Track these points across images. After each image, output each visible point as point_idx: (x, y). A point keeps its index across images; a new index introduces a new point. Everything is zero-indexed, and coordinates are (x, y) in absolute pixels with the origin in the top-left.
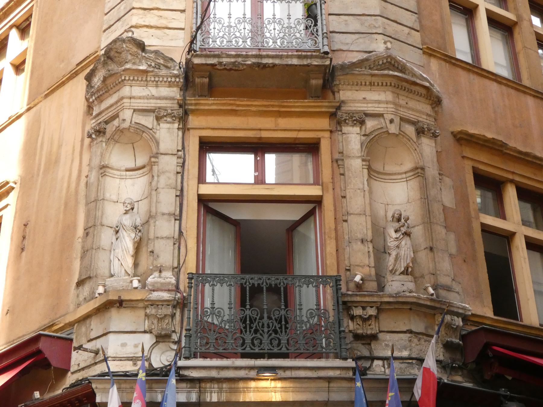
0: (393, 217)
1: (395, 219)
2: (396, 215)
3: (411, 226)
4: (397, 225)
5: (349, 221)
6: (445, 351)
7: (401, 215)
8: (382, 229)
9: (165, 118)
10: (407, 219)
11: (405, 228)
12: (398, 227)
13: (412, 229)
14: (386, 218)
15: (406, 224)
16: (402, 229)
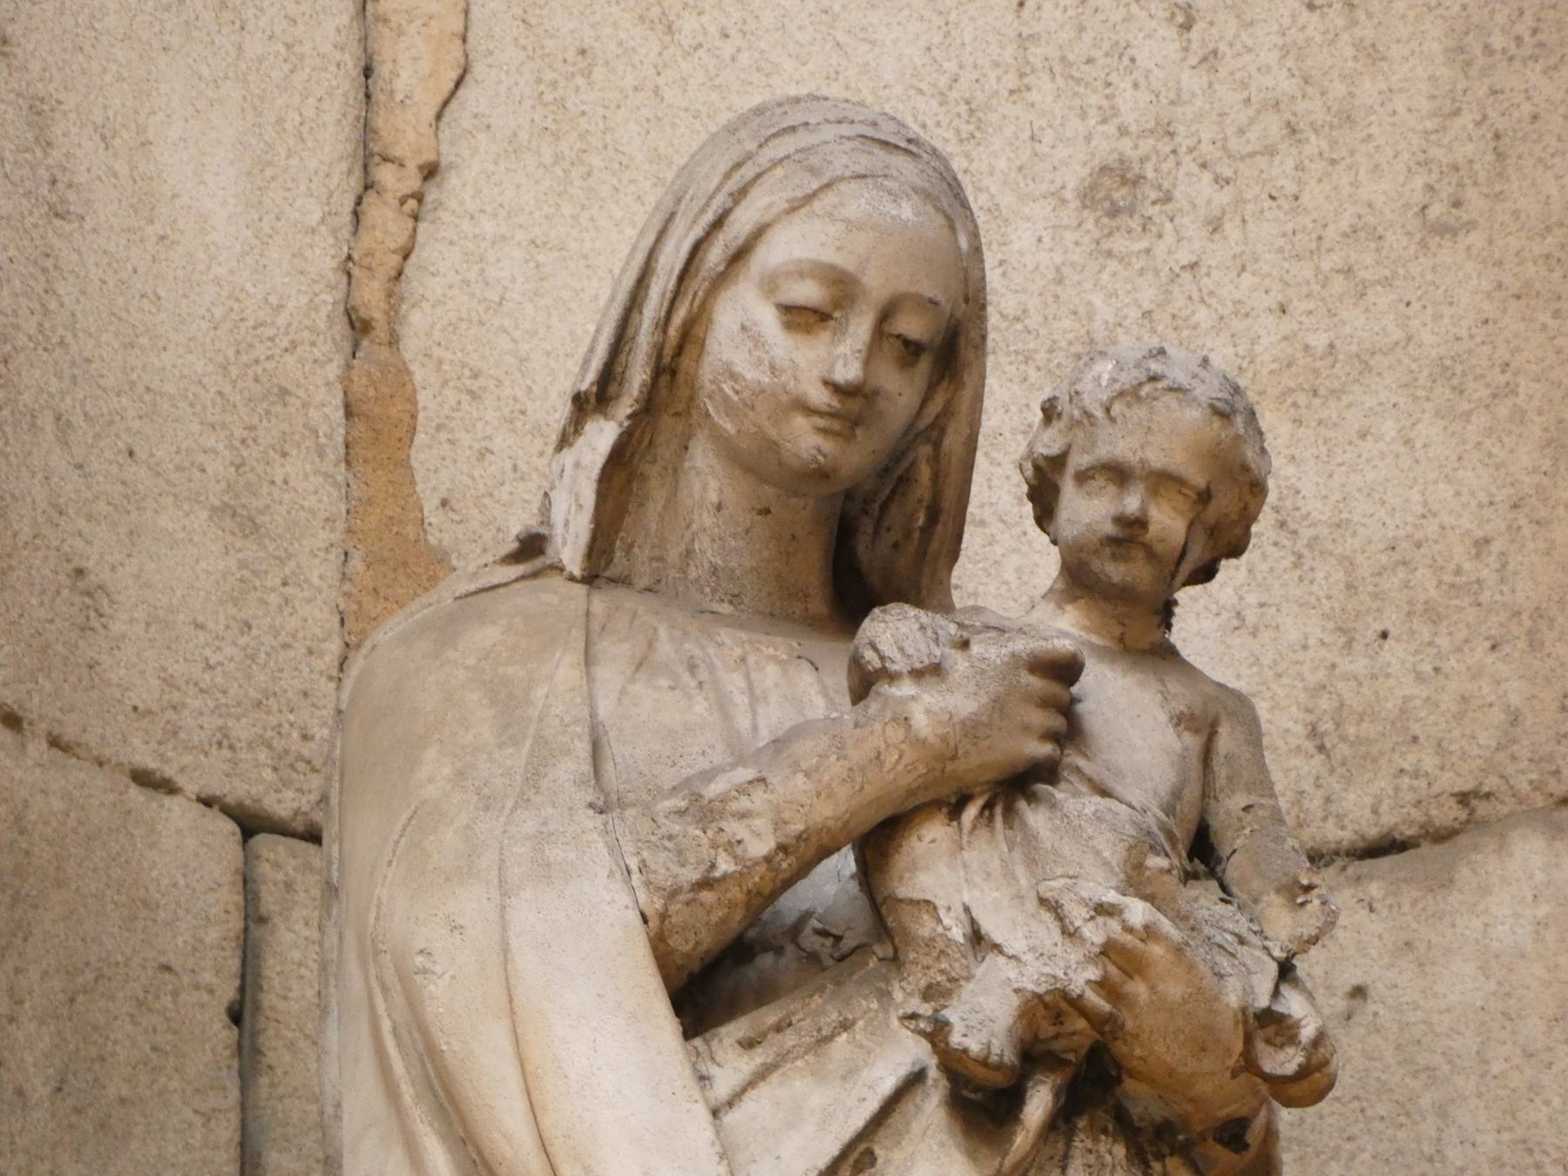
0: (647, 391)
1: (704, 493)
2: (753, 347)
3: (1304, 791)
4: (754, 724)
5: (331, 846)
6: (1060, 586)
7: (945, 349)
8: (188, 853)
9: (1259, 1080)
10: (1162, 540)
11: (1083, 844)
12: (813, 792)
13: (1363, 929)
14: (376, 427)
15: (1118, 701)
16: (950, 874)
